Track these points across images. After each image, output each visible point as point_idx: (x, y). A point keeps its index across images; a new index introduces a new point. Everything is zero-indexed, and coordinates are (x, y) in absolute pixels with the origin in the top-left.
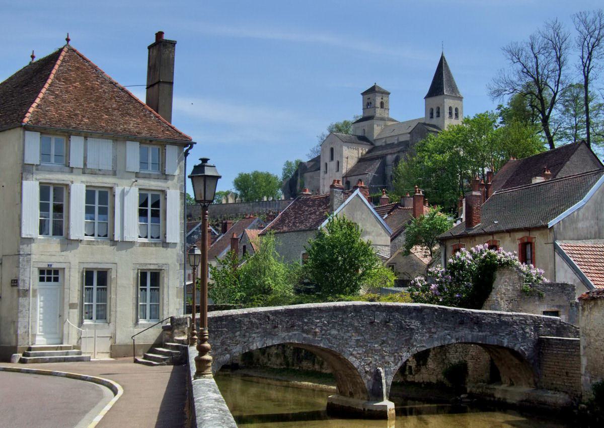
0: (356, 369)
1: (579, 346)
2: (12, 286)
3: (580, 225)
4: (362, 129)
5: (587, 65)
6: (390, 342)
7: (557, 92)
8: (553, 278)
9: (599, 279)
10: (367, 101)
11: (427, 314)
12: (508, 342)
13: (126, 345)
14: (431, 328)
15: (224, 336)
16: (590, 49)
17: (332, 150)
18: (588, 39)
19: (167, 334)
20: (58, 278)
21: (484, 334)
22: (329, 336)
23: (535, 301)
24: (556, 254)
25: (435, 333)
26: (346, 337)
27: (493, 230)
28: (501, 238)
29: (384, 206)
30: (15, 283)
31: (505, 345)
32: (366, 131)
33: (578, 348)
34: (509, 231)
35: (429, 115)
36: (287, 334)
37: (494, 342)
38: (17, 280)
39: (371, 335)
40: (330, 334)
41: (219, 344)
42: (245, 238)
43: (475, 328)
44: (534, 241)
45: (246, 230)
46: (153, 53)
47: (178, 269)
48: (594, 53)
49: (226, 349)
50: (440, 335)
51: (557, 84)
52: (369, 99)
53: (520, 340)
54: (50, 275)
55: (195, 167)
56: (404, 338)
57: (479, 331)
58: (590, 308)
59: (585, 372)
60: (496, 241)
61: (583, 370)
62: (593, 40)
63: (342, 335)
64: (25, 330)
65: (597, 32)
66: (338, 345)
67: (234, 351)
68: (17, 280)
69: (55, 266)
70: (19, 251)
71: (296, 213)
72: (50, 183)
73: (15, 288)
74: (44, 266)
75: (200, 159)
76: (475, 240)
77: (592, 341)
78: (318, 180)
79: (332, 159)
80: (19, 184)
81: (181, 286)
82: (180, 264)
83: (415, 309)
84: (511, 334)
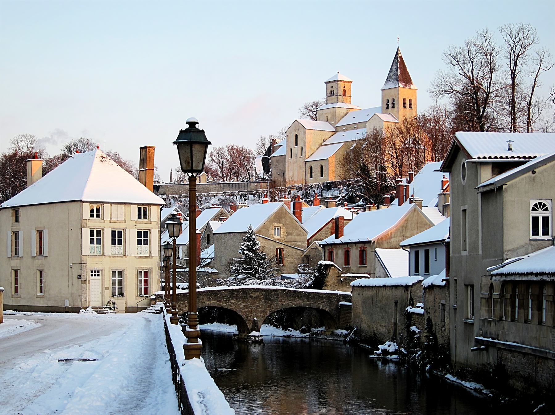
2: (78, 278)
3: (392, 240)
4: (326, 116)
6: (261, 306)
10: (330, 89)
13: (135, 307)
15: (179, 303)
17: (296, 136)
18: (514, 49)
20: (99, 274)
23: (346, 286)
25: (284, 302)
26: (238, 304)
30: (79, 277)
37: (315, 306)
38: (80, 276)
40: (230, 302)
42: (209, 226)
46: (142, 151)
49: (181, 309)
54: (95, 273)
57: (307, 301)
60: (349, 248)
63: (237, 303)
64: (85, 300)
66: (235, 308)
67: (184, 310)
68: (80, 276)
69: (98, 269)
70: (81, 262)
72: (95, 228)
73: (80, 280)
74: (93, 269)
78: (284, 165)
80: (80, 229)
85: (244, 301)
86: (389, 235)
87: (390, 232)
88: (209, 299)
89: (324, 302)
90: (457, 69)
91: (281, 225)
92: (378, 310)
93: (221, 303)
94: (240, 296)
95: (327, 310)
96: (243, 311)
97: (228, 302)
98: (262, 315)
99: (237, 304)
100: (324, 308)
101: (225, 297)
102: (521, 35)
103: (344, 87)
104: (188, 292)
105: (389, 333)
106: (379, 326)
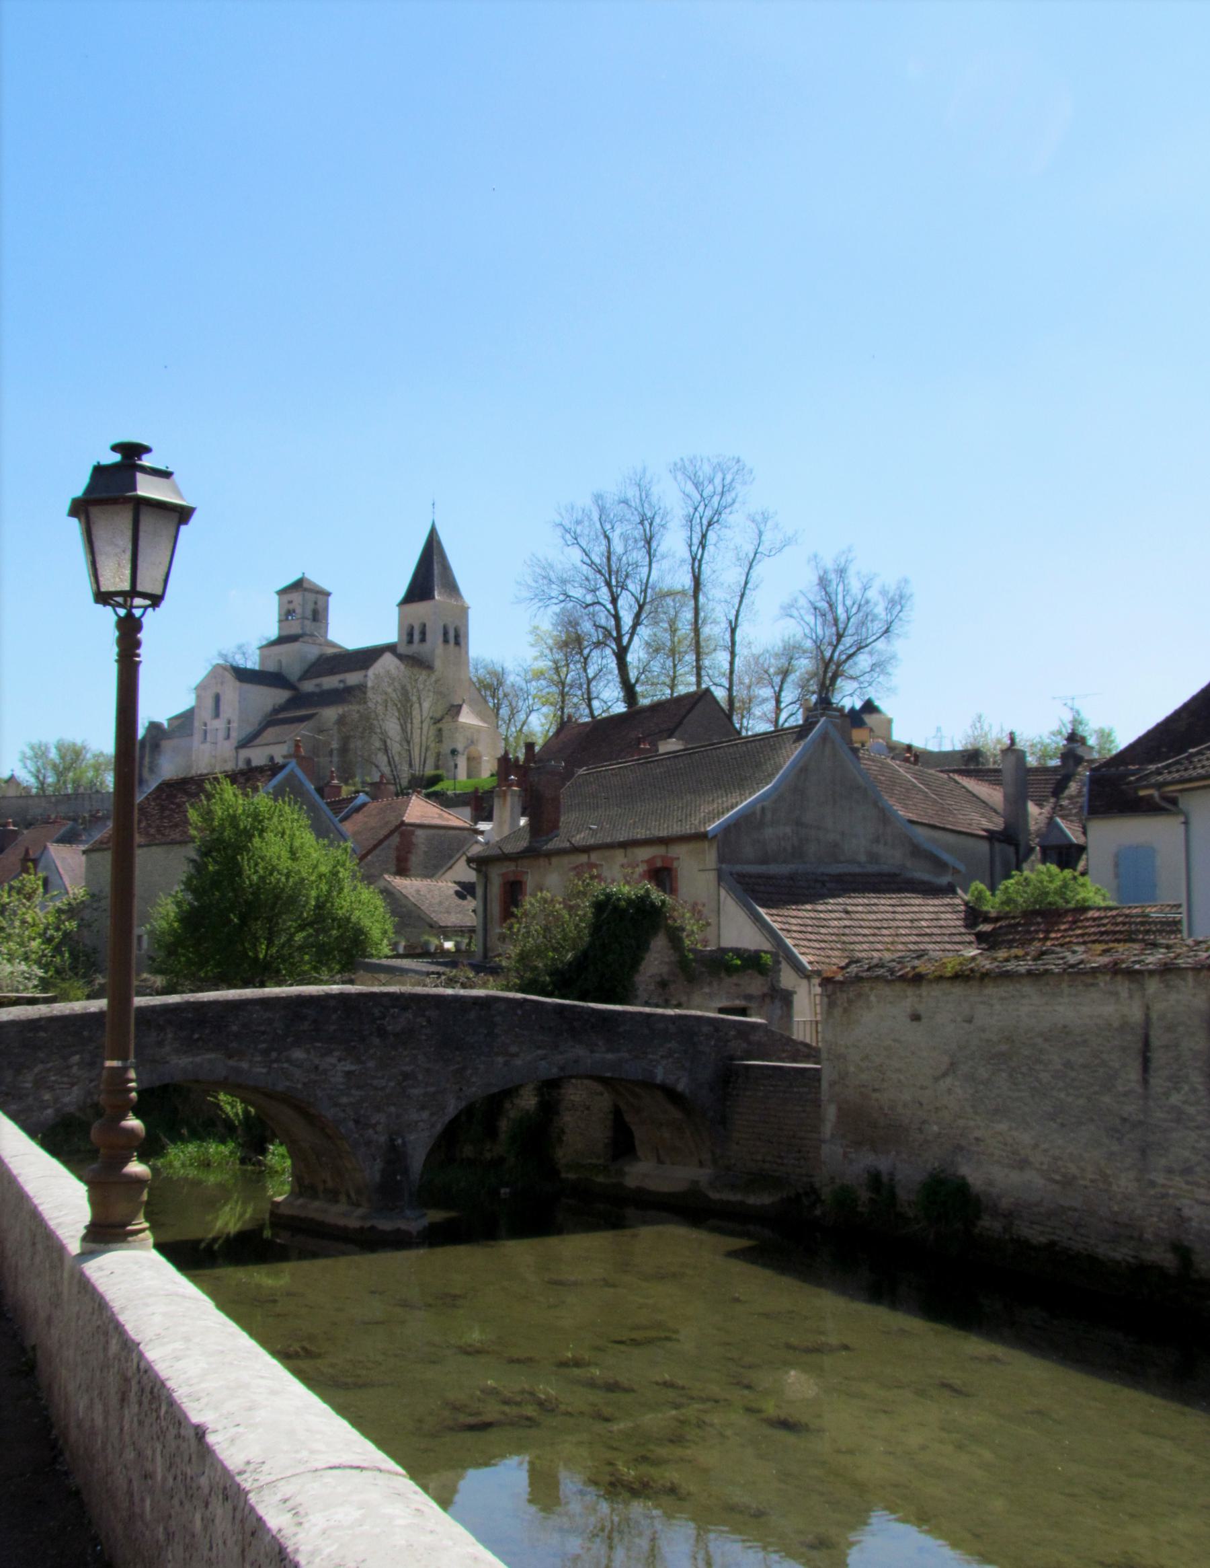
1: (819, 1080)
3: (769, 832)
5: (699, 557)
6: (420, 1077)
7: (644, 603)
9: (806, 943)
10: (286, 607)
16: (704, 528)
18: (701, 509)
22: (286, 1065)
24: (723, 893)
27: (592, 841)
29: (335, 801)
31: (659, 1078)
33: (817, 1084)
34: (625, 845)
35: (405, 638)
36: (191, 1060)
40: (289, 1060)
41: (28, 1085)
43: (600, 1043)
44: (675, 864)
45: (48, 844)
48: (712, 536)
51: (643, 588)
52: (290, 602)
53: (29, 1035)
56: (452, 1068)
58: (850, 1001)
59: (833, 1136)
61: (827, 1129)
62: (709, 513)
63: (317, 1062)
65: (716, 499)
71: (163, 809)
75: (115, 448)
76: (550, 864)
77: (852, 1069)
79: (217, 714)
83: (474, 1004)
86: (758, 816)
87: (759, 806)
90: (576, 555)
94: (333, 1028)
96: (344, 1100)
97: (277, 1060)
98: (425, 1115)
99: (317, 1068)
101: (264, 1033)
102: (717, 481)
104: (1059, 764)
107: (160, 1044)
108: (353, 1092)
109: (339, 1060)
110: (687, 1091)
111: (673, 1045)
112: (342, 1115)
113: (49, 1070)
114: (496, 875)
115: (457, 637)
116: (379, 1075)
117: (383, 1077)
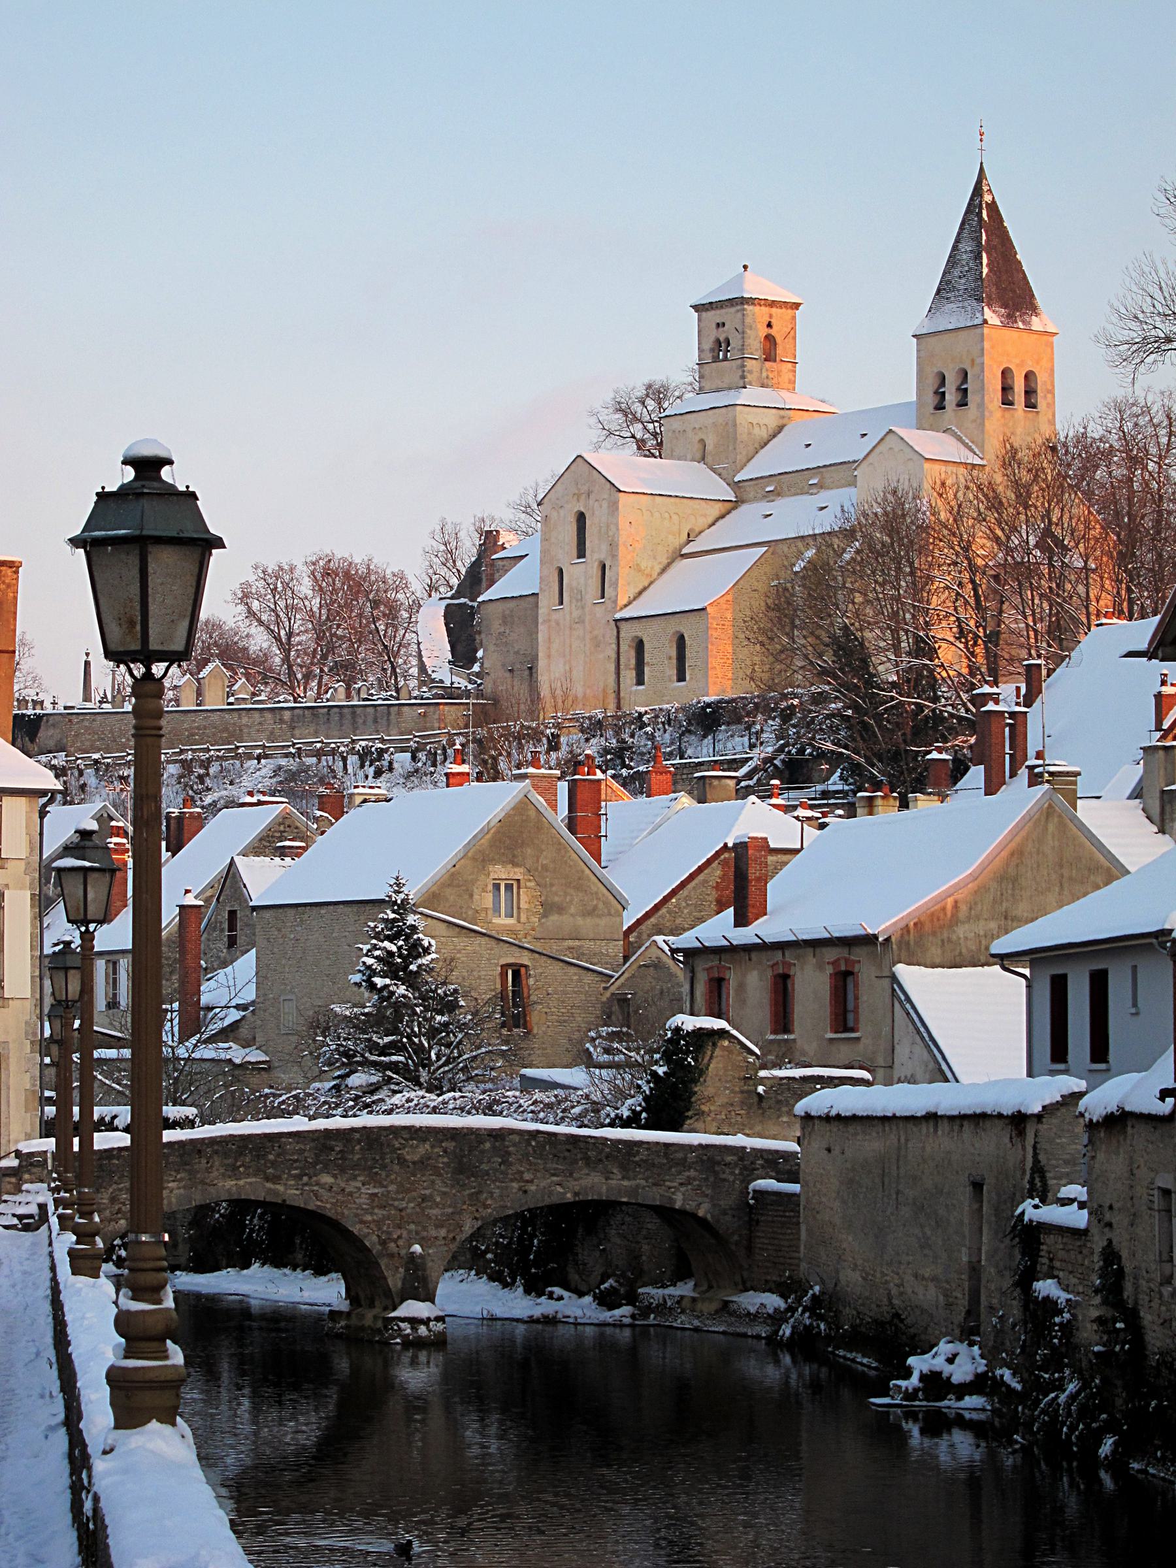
0: (369, 1250)
3: (961, 931)
6: (438, 1199)
8: (889, 1059)
10: (713, 334)
11: (514, 1145)
12: (684, 1200)
14: (522, 1172)
17: (581, 518)
19: (10, 1183)
21: (633, 1183)
22: (315, 1188)
25: (531, 1181)
28: (798, 958)
32: (709, 448)
36: (233, 1183)
39: (401, 1185)
40: (317, 1184)
42: (234, 876)
43: (615, 1171)
47: (29, 1051)
50: (542, 1185)
55: (102, 496)
56: (468, 1192)
57: (623, 1178)
60: (790, 965)
63: (343, 1185)
78: (533, 633)
81: (34, 1085)
82: (32, 1042)
84: (690, 1184)
85: (374, 1179)
86: (949, 914)
87: (950, 901)
88: (233, 1171)
89: (689, 1181)
91: (518, 873)
92: (906, 1212)
93: (281, 1188)
94: (358, 1156)
95: (701, 1213)
96: (369, 1218)
99: (343, 1190)
100: (690, 1206)
103: (769, 325)
105: (949, 1305)
106: (909, 1278)
107: (208, 1170)
108: (376, 1211)
109: (363, 1184)
110: (709, 1217)
111: (692, 1173)
112: (366, 1231)
113: (120, 1190)
114: (701, 965)
115: (1030, 392)
116: (400, 1196)
117: (403, 1200)
